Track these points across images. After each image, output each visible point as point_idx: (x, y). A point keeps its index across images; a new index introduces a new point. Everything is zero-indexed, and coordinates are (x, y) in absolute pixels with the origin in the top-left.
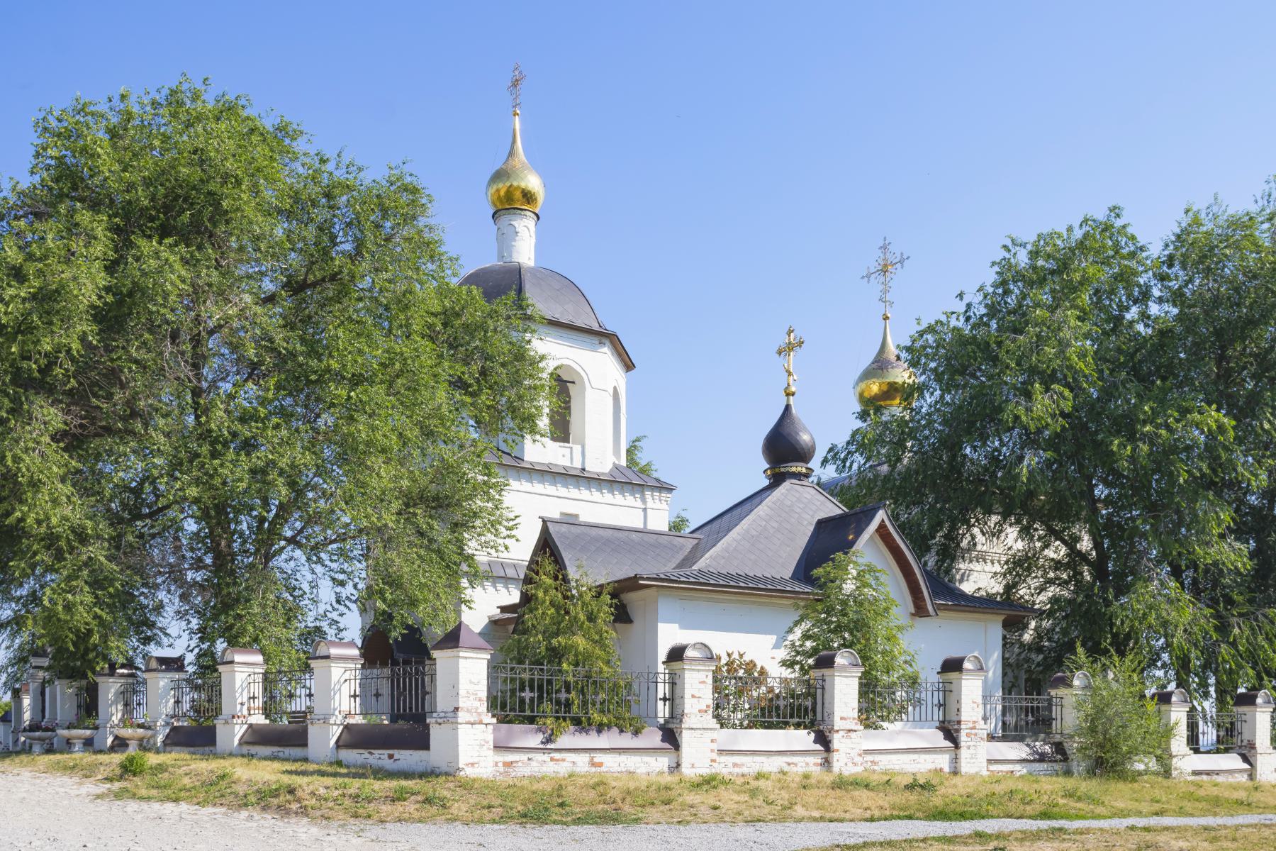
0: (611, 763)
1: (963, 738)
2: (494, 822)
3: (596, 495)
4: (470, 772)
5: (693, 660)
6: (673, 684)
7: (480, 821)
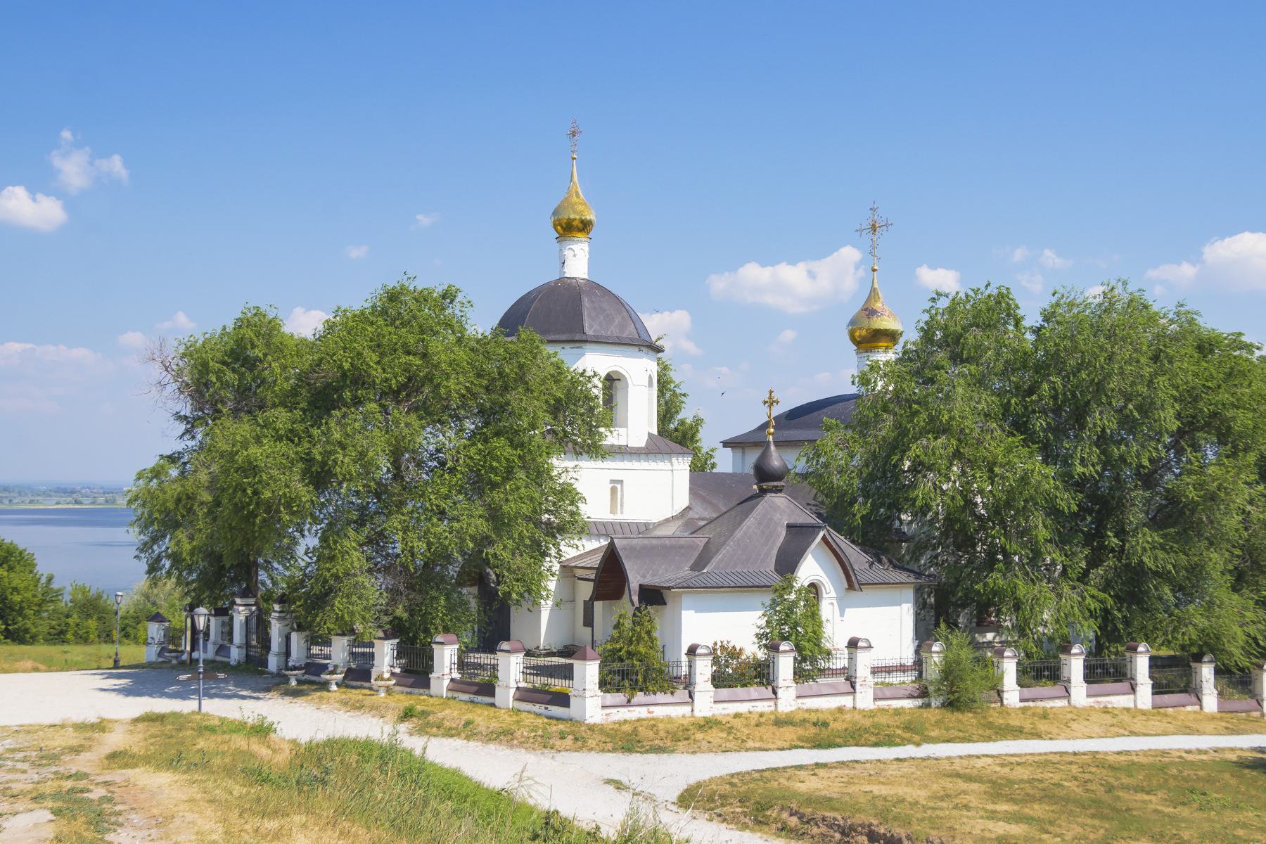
0: (659, 712)
1: (858, 687)
2: (609, 751)
3: (635, 464)
4: (589, 721)
5: (700, 655)
6: (690, 666)
7: (603, 751)
